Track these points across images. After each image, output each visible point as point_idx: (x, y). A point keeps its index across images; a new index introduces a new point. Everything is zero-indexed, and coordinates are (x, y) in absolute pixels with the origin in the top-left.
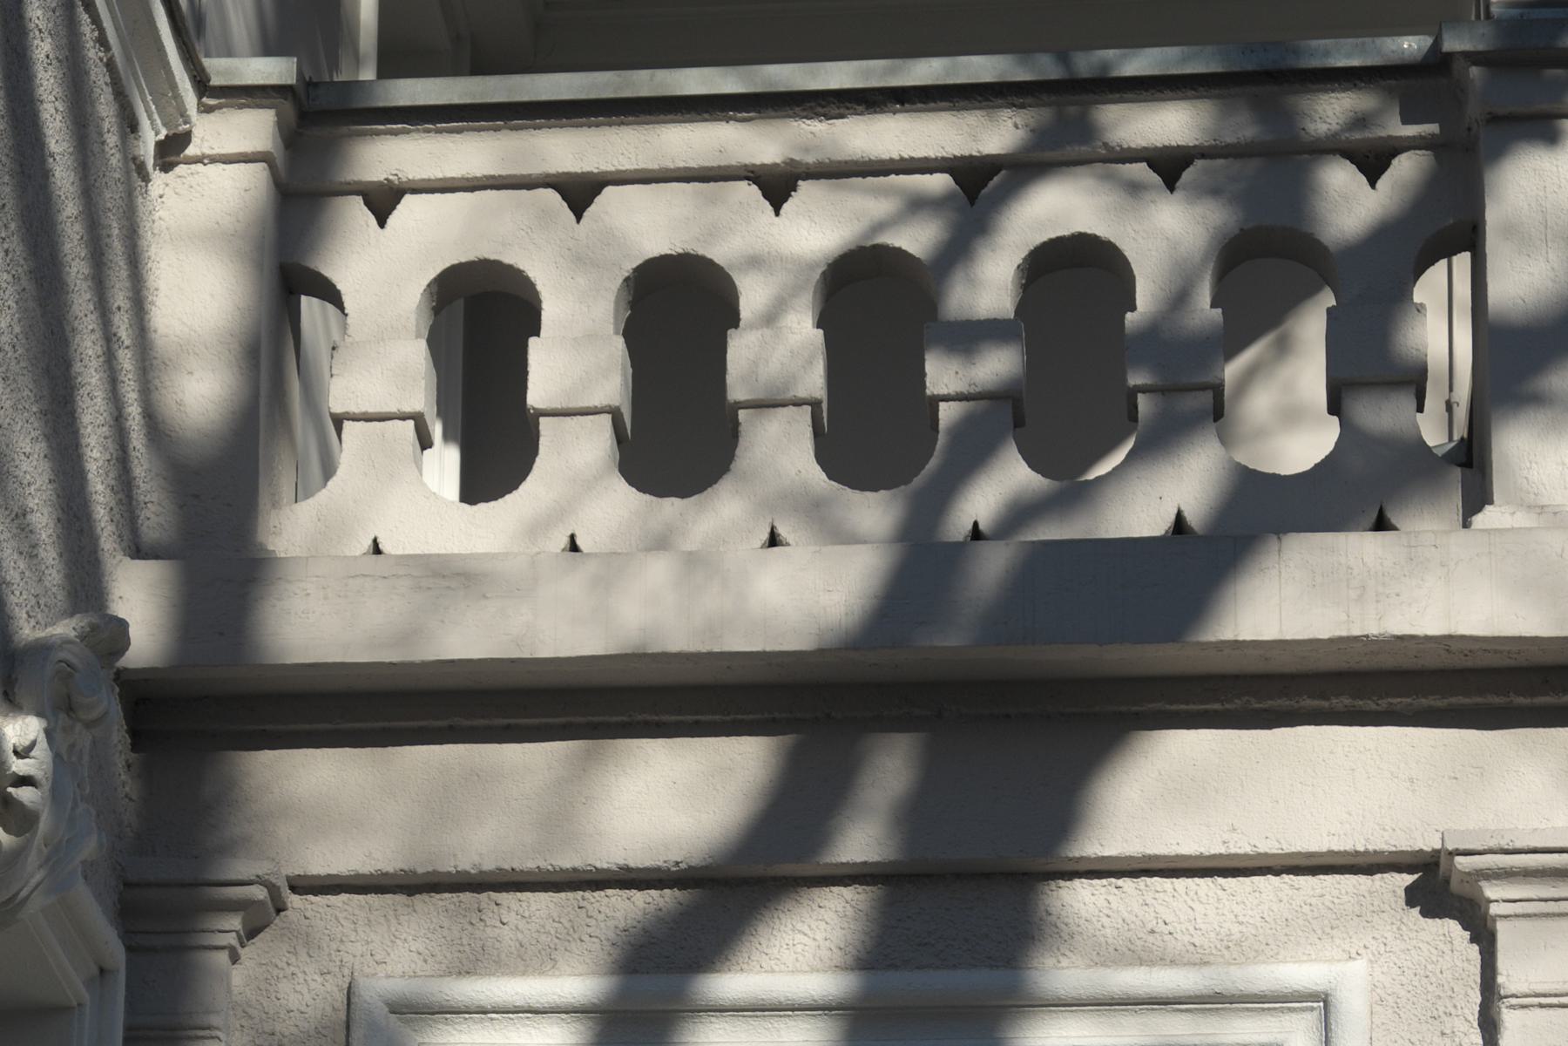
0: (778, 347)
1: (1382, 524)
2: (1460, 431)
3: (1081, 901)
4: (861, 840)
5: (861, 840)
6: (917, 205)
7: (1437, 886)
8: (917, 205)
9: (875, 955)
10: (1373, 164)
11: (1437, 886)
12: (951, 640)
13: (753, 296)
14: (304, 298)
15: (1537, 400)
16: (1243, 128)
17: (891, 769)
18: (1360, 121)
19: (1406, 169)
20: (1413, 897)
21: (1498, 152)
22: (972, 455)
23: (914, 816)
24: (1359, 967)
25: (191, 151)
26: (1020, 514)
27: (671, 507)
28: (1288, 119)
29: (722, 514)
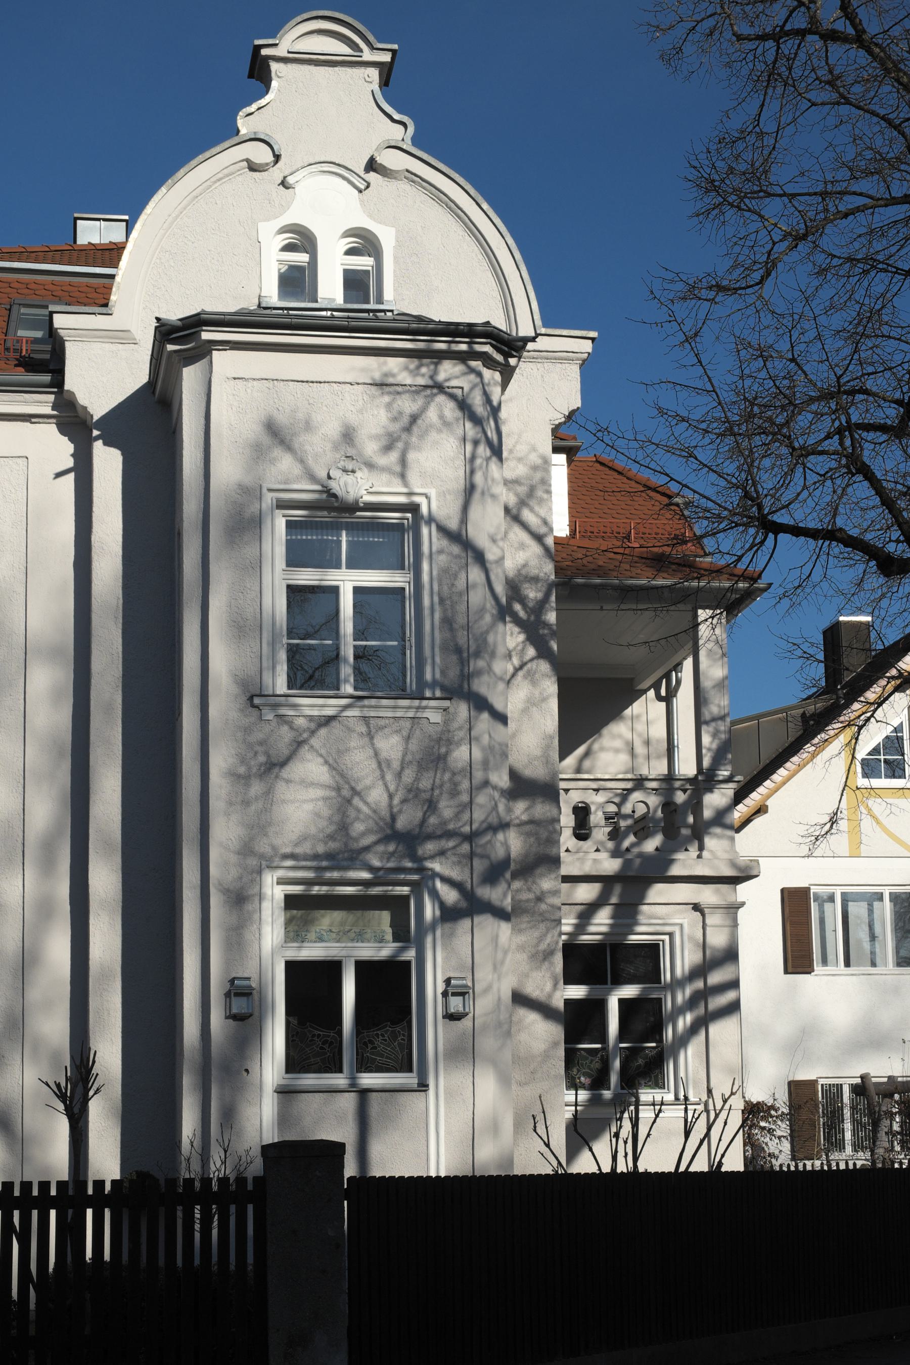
0: (596, 818)
1: (686, 850)
2: (447, 390)
3: (644, 908)
4: (614, 900)
5: (614, 900)
6: (617, 795)
7: (696, 907)
8: (617, 795)
9: (614, 916)
10: (685, 791)
11: (696, 907)
12: (630, 874)
13: (593, 808)
14: (742, 1169)
15: (709, 833)
16: (664, 786)
17: (618, 889)
18: (683, 785)
19: (689, 792)
20: (693, 908)
21: (704, 794)
22: (626, 836)
23: (621, 896)
24: (686, 920)
25: (579, 908)
26: (633, 845)
27: (582, 842)
28: (671, 785)
29: (588, 845)
